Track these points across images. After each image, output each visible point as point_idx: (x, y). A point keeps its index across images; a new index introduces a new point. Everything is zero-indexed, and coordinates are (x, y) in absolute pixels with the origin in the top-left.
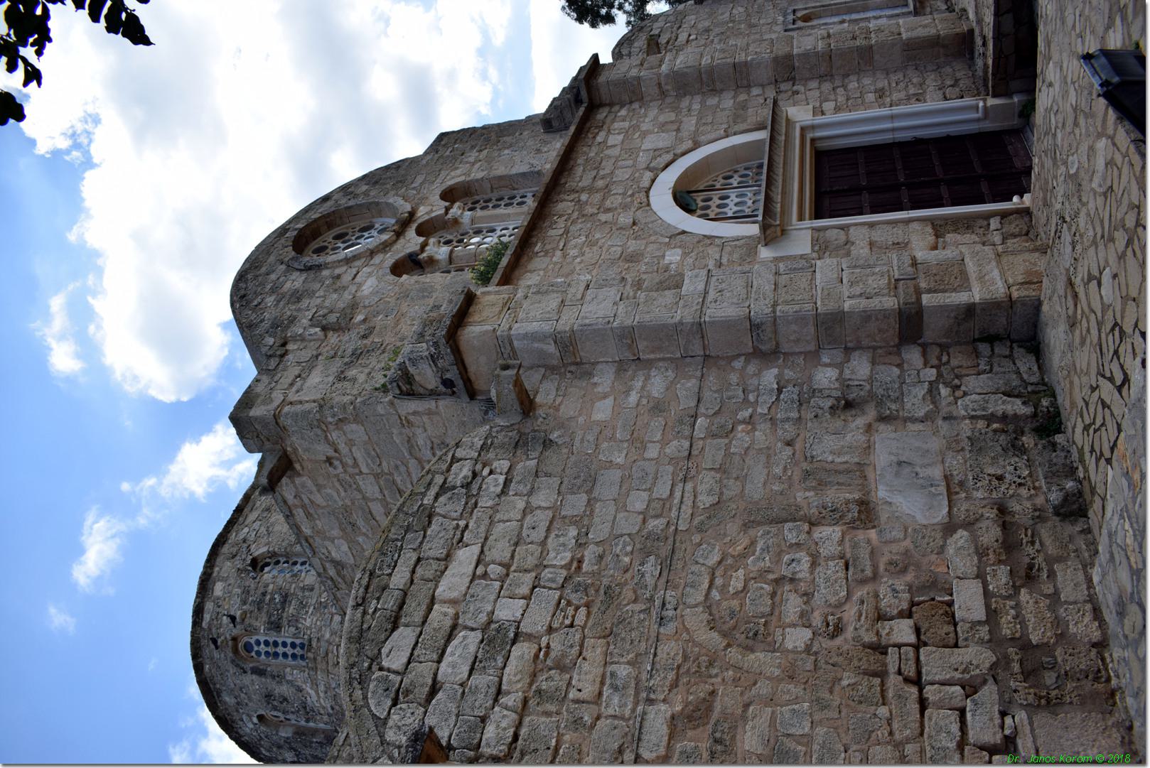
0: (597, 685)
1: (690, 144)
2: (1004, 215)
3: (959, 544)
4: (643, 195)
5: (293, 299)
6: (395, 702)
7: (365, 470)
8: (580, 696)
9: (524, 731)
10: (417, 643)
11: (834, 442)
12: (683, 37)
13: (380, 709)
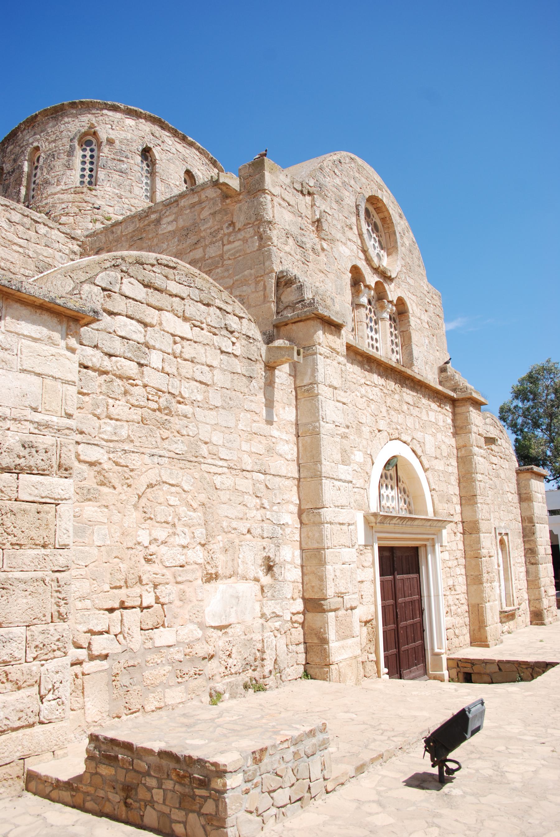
0: (117, 417)
1: (427, 466)
2: (377, 663)
3: (194, 632)
4: (396, 436)
5: (337, 198)
6: (104, 290)
7: (226, 248)
8: (110, 407)
9: (90, 372)
10: (137, 301)
11: (250, 559)
12: (494, 460)
13: (100, 280)
